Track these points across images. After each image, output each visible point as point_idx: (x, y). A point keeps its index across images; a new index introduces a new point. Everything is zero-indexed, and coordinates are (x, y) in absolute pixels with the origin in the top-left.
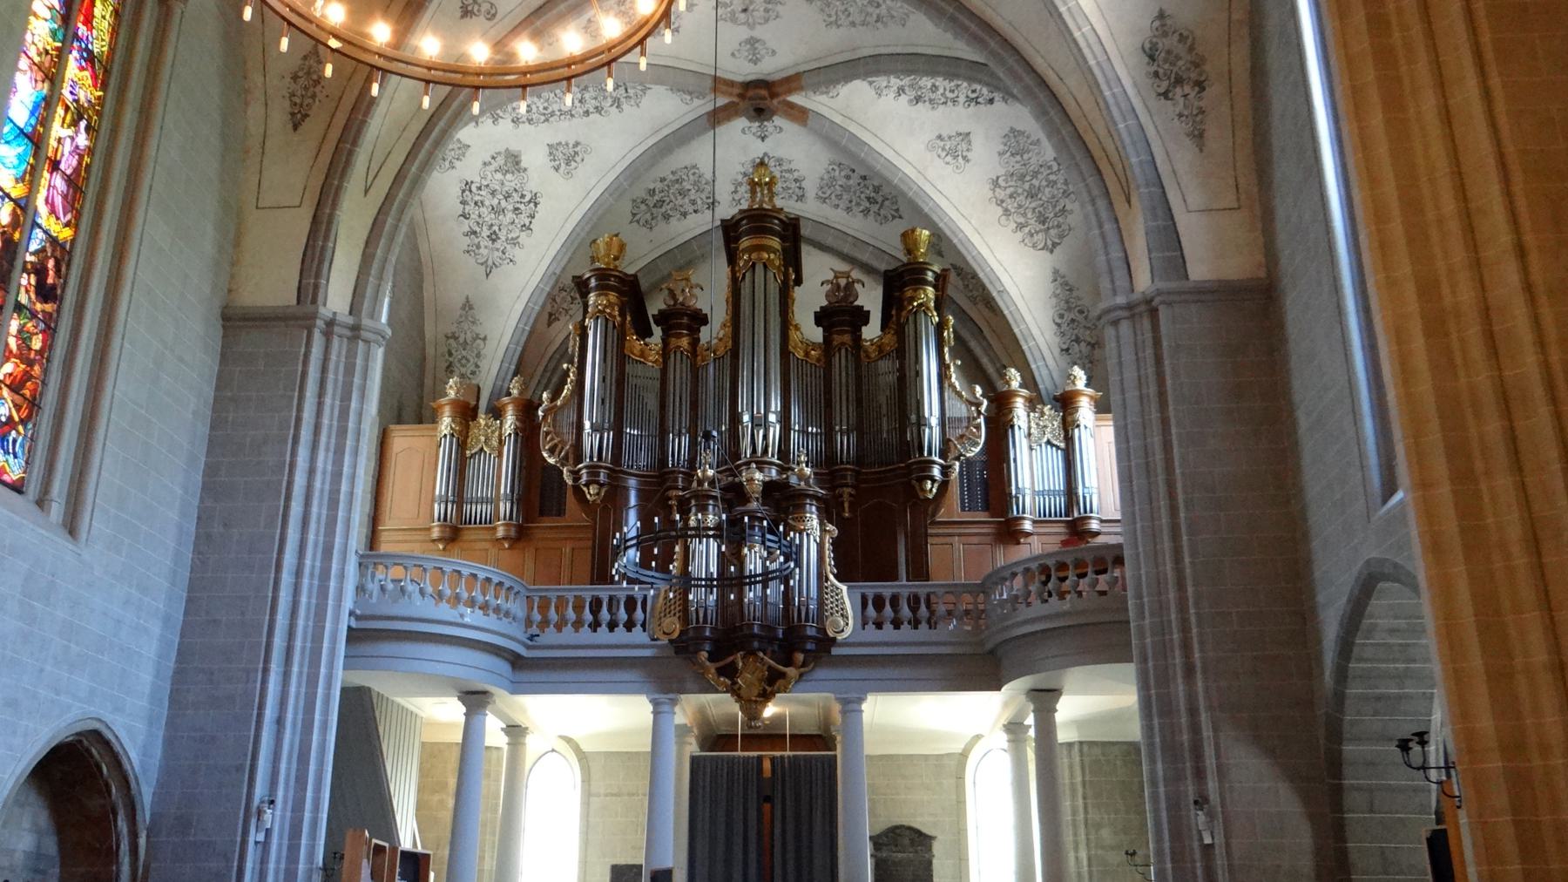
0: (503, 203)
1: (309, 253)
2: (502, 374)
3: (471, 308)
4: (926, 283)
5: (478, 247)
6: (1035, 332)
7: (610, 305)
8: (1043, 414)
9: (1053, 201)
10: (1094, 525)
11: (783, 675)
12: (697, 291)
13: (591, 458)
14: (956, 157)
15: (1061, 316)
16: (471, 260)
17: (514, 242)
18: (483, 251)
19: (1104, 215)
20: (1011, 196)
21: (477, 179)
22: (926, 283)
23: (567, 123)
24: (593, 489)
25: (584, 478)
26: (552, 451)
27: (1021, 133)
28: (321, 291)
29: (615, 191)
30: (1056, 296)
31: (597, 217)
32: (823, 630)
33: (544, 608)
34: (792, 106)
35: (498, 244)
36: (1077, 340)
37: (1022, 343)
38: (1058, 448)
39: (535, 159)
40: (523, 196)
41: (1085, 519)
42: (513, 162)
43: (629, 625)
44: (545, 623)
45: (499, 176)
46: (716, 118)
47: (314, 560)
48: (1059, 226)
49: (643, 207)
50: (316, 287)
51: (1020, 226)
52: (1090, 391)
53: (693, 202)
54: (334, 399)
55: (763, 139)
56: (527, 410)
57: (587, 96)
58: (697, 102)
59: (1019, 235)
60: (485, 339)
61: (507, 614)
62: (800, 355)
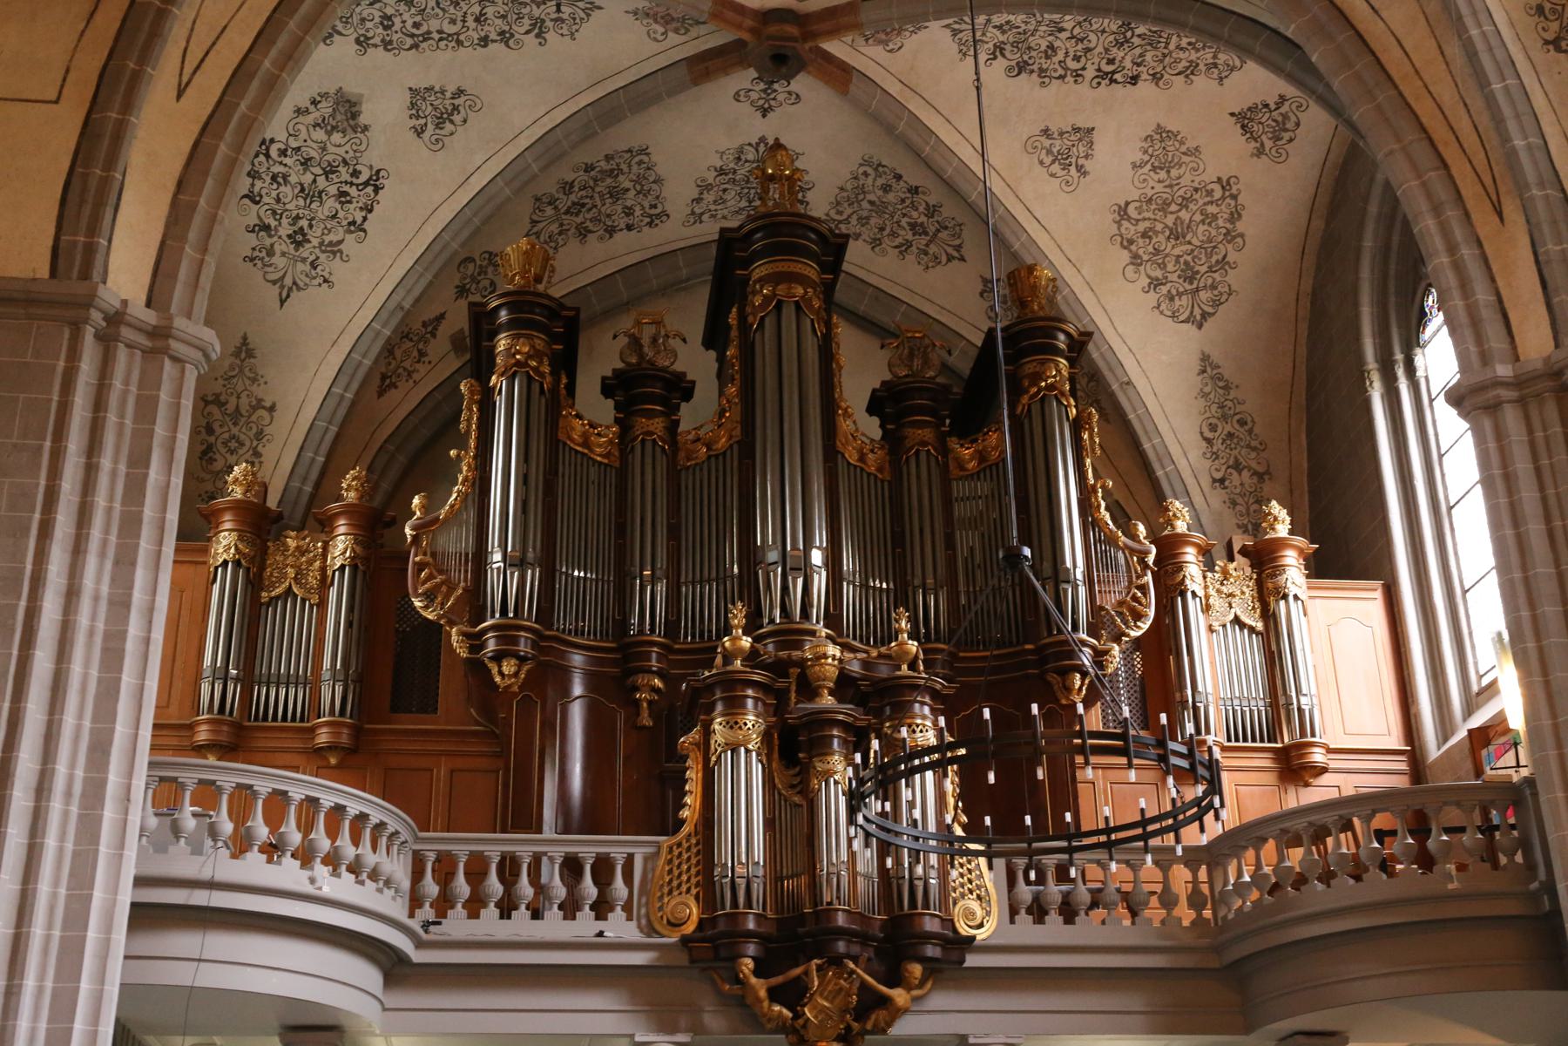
0: (321, 182)
1: (76, 181)
2: (301, 470)
3: (251, 354)
4: (1056, 351)
5: (271, 253)
6: (1175, 450)
7: (535, 354)
8: (1226, 574)
9: (1209, 246)
10: (1318, 756)
11: (885, 1001)
12: (675, 343)
13: (504, 612)
14: (1066, 167)
15: (1213, 428)
16: (256, 274)
17: (334, 249)
18: (279, 261)
19: (1459, 234)
20: (1144, 235)
21: (282, 136)
22: (1056, 351)
23: (449, 54)
24: (508, 667)
25: (491, 646)
26: (429, 597)
27: (1172, 135)
28: (99, 258)
29: (516, 175)
30: (1205, 395)
31: (486, 212)
32: (949, 923)
33: (445, 876)
34: (828, 58)
35: (305, 252)
36: (1237, 467)
37: (1156, 466)
38: (1252, 630)
39: (385, 111)
40: (356, 174)
41: (1302, 747)
42: (346, 112)
43: (601, 908)
44: (444, 904)
45: (319, 135)
46: (704, 67)
47: (72, 765)
48: (1213, 287)
49: (549, 211)
50: (90, 250)
51: (1155, 284)
52: (1300, 541)
53: (628, 212)
54: (116, 461)
55: (765, 112)
56: (376, 525)
57: (490, 11)
58: (674, 38)
59: (1152, 297)
60: (272, 409)
61: (374, 875)
62: (853, 458)
